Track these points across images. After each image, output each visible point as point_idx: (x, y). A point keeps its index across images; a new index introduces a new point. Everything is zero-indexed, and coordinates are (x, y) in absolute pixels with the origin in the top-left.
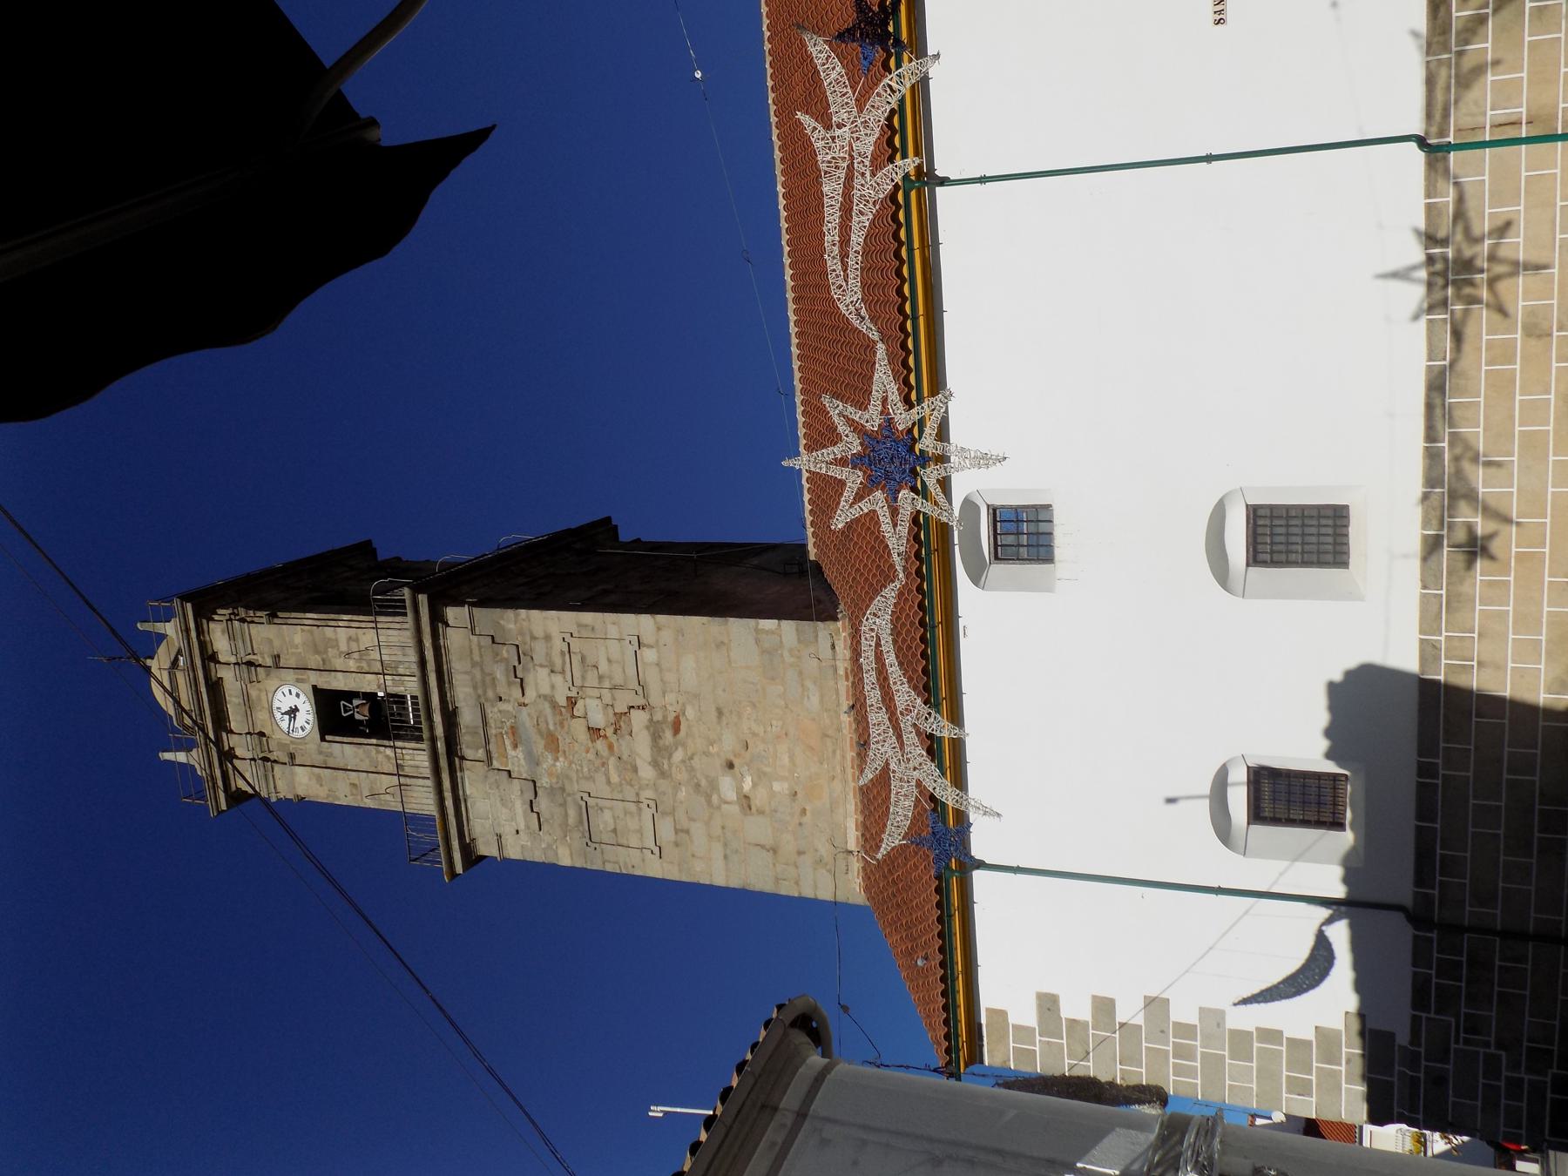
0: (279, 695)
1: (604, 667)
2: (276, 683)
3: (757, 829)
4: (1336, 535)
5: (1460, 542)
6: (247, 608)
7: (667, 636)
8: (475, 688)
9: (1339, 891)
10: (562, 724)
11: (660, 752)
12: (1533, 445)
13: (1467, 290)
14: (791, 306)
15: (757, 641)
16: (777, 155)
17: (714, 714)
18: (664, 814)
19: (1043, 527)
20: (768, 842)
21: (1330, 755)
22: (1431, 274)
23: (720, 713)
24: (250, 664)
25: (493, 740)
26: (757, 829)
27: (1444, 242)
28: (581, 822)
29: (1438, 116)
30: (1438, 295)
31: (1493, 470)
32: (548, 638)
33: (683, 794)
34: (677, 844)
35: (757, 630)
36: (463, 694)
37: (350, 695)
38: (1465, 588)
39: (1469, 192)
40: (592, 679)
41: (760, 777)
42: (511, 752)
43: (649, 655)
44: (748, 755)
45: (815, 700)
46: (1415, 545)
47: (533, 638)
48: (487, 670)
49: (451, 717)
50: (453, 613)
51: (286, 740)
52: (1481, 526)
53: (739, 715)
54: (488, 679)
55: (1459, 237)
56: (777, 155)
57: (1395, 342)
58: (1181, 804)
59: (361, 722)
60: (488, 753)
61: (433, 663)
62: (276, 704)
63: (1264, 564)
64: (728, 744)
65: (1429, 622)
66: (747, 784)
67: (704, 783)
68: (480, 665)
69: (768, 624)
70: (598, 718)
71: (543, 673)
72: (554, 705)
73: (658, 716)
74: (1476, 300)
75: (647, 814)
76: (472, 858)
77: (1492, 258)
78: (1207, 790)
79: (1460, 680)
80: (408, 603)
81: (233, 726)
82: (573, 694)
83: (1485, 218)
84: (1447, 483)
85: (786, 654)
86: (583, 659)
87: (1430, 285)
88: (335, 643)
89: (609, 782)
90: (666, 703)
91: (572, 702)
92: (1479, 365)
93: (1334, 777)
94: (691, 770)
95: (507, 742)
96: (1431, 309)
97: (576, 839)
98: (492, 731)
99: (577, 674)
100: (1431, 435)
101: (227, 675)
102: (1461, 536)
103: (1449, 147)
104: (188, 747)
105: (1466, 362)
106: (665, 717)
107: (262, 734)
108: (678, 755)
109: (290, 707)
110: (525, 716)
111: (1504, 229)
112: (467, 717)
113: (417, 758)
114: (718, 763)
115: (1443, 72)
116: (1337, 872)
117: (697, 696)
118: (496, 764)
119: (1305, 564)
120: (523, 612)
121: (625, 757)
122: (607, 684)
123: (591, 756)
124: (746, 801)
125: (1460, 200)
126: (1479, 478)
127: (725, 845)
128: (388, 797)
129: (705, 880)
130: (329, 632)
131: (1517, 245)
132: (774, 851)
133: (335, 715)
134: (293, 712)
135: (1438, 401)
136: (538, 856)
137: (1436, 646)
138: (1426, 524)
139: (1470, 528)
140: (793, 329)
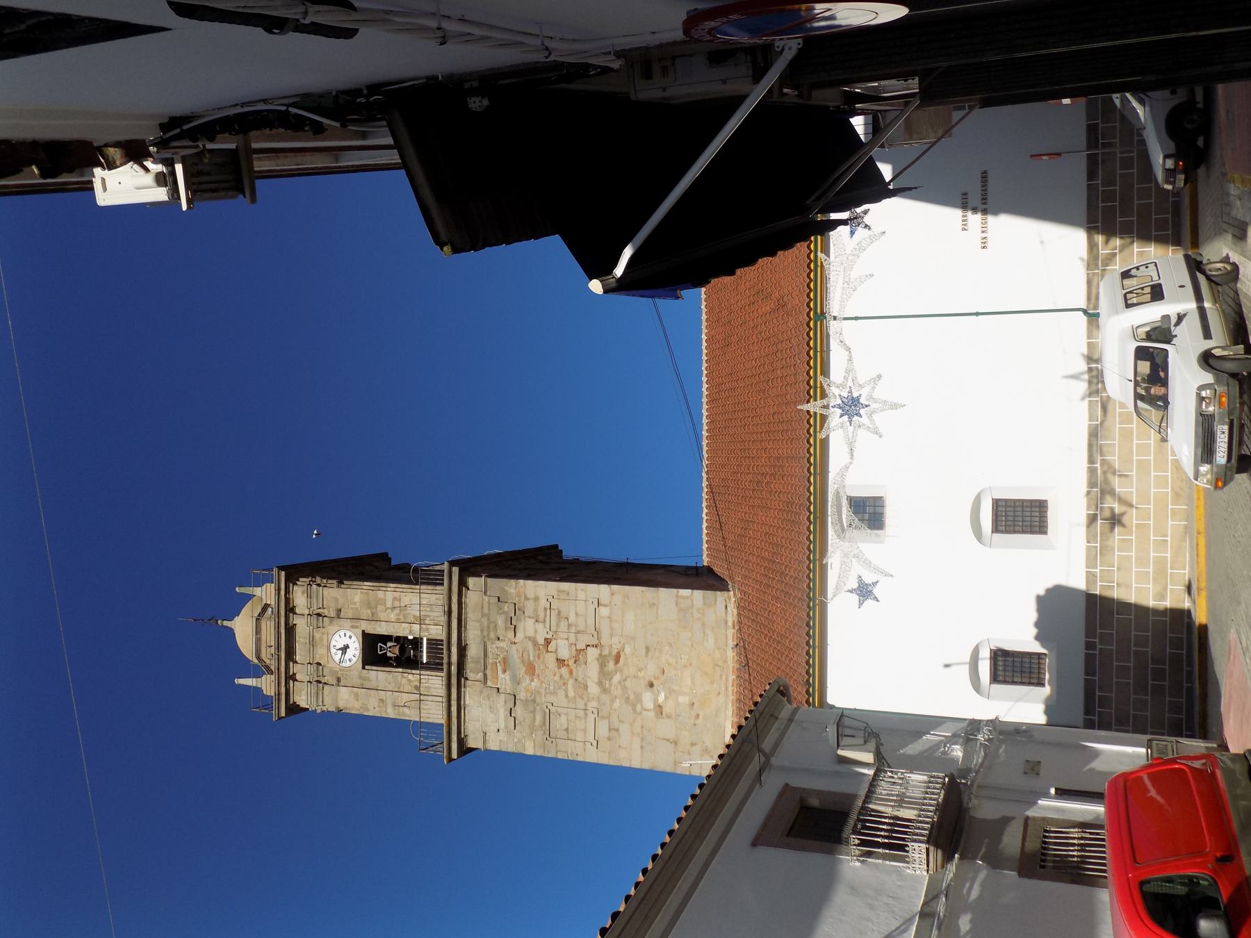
0: (336, 636)
1: (572, 619)
2: (336, 628)
3: (666, 728)
5: (1107, 518)
7: (618, 599)
8: (482, 631)
11: (604, 675)
12: (1143, 467)
14: (705, 406)
16: (704, 317)
17: (644, 651)
18: (603, 718)
20: (671, 736)
21: (1037, 638)
23: (648, 649)
24: (319, 615)
26: (666, 728)
28: (544, 724)
30: (1094, 387)
31: (1123, 479)
32: (536, 599)
33: (617, 704)
34: (609, 739)
35: (677, 596)
37: (385, 639)
38: (1109, 543)
41: (671, 693)
42: (501, 675)
43: (604, 611)
44: (663, 678)
45: (711, 641)
46: (1083, 519)
47: (526, 599)
49: (462, 650)
50: (472, 581)
52: (1118, 509)
53: (661, 652)
54: (492, 626)
56: (704, 317)
59: (391, 658)
61: (456, 615)
62: (333, 643)
63: (1001, 532)
64: (651, 671)
65: (1091, 561)
66: (661, 698)
67: (632, 697)
68: (488, 616)
69: (685, 592)
70: (564, 653)
71: (530, 623)
72: (535, 644)
73: (606, 652)
75: (591, 717)
76: (464, 750)
78: (968, 660)
79: (1108, 594)
80: (446, 573)
81: (298, 658)
82: (549, 636)
84: (1100, 486)
86: (559, 613)
87: (1090, 382)
88: (383, 602)
89: (567, 696)
90: (612, 642)
93: (1039, 655)
94: (625, 688)
95: (499, 668)
96: (1090, 395)
97: (539, 736)
98: (490, 661)
99: (554, 623)
100: (1091, 460)
101: (301, 624)
102: (1107, 514)
104: (257, 674)
105: (1106, 424)
106: (610, 653)
107: (319, 664)
108: (617, 678)
109: (344, 645)
110: (514, 652)
112: (473, 651)
113: (434, 682)
114: (643, 683)
116: (1042, 707)
117: (633, 638)
118: (489, 683)
119: (1023, 532)
120: (522, 581)
121: (580, 679)
122: (573, 630)
123: (557, 678)
124: (659, 709)
126: (1116, 483)
127: (642, 739)
128: (406, 710)
129: (626, 764)
130: (380, 594)
132: (676, 743)
133: (375, 651)
134: (345, 649)
136: (511, 748)
137: (1094, 575)
138: (1089, 508)
139: (1112, 509)
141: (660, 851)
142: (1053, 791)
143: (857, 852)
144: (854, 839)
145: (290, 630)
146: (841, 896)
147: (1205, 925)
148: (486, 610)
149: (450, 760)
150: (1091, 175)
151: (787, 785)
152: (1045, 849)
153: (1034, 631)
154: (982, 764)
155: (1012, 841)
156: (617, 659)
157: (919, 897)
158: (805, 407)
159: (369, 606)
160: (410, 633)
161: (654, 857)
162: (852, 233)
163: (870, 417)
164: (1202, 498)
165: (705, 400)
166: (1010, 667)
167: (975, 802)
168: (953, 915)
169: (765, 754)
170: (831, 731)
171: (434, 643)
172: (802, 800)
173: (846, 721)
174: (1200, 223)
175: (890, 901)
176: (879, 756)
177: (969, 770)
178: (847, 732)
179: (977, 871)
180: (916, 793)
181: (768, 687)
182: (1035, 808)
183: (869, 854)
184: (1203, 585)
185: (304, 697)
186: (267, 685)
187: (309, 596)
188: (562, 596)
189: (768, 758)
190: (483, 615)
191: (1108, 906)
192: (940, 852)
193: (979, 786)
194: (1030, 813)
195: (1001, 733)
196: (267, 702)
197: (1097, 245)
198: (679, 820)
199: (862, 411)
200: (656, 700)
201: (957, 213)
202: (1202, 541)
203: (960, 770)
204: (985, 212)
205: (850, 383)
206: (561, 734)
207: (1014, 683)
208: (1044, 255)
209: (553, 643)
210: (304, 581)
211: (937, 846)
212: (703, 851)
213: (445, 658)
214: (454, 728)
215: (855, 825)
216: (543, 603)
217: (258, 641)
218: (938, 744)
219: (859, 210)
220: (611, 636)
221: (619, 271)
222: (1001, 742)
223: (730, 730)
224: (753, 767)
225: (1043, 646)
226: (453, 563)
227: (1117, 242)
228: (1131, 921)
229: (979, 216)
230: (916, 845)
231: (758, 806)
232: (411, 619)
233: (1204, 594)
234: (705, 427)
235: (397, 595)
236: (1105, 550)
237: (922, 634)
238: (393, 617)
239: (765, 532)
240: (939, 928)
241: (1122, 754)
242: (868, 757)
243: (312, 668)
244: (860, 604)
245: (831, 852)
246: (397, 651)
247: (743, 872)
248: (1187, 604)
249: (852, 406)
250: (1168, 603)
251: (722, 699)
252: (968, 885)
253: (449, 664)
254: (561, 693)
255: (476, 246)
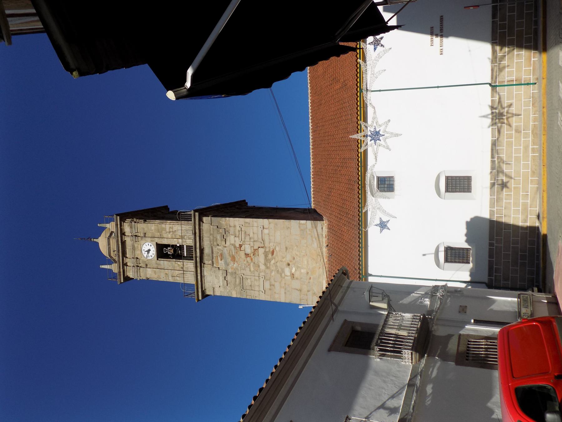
0: (144, 245)
1: (251, 235)
2: (144, 242)
3: (296, 284)
4: (468, 184)
5: (500, 184)
6: (137, 219)
7: (272, 226)
8: (210, 242)
9: (468, 279)
10: (237, 253)
11: (267, 260)
12: (517, 159)
13: (501, 120)
14: (311, 134)
15: (299, 227)
16: (309, 91)
18: (267, 280)
19: (391, 183)
20: (298, 288)
21: (466, 241)
22: (493, 116)
23: (286, 248)
24: (136, 236)
25: (214, 258)
26: (296, 284)
27: (496, 109)
28: (240, 283)
29: (494, 79)
30: (494, 121)
31: (508, 165)
32: (235, 226)
33: (273, 274)
34: (270, 289)
35: (299, 224)
36: (206, 244)
37: (167, 246)
38: (501, 196)
39: (502, 97)
40: (248, 238)
41: (298, 268)
42: (220, 262)
43: (266, 231)
44: (294, 262)
46: (488, 185)
47: (230, 226)
48: (215, 236)
49: (202, 251)
50: (205, 219)
51: (145, 260)
52: (505, 179)
54: (215, 239)
55: (499, 107)
56: (309, 91)
57: (484, 133)
58: (427, 256)
60: (213, 262)
61: (198, 235)
62: (143, 248)
64: (288, 258)
65: (492, 205)
66: (293, 271)
67: (280, 270)
69: (303, 222)
70: (248, 251)
71: (232, 237)
72: (235, 247)
73: (267, 250)
74: (503, 123)
75: (262, 280)
76: (205, 296)
77: (507, 112)
78: (434, 252)
79: (500, 220)
82: (241, 243)
83: (505, 103)
84: (496, 169)
85: (308, 231)
86: (245, 233)
87: (492, 119)
89: (250, 270)
90: (270, 245)
91: (241, 246)
92: (504, 140)
94: (276, 266)
95: (219, 259)
96: (492, 125)
97: (238, 289)
98: (215, 255)
99: (243, 237)
100: (493, 157)
101: (128, 240)
102: (500, 182)
103: (496, 86)
104: (110, 263)
105: (500, 139)
106: (269, 250)
107: (137, 258)
108: (273, 262)
109: (148, 249)
110: (226, 251)
111: (510, 106)
112: (207, 251)
113: (190, 265)
114: (285, 264)
115: (496, 68)
116: (468, 273)
117: (280, 244)
118: (215, 265)
120: (228, 219)
122: (252, 240)
123: (245, 262)
124: (293, 275)
125: (500, 98)
126: (504, 167)
127: (285, 289)
128: (178, 278)
130: (163, 226)
131: (513, 110)
132: (300, 290)
133: (163, 252)
134: (149, 251)
135: (494, 148)
136: (226, 294)
137: (493, 211)
138: (491, 179)
139: (502, 180)
140: (311, 141)
141: (283, 356)
142: (472, 321)
143: (378, 354)
144: (377, 348)
145: (123, 243)
146: (370, 376)
147: (549, 416)
148: (212, 232)
149: (198, 300)
150: (494, 16)
151: (346, 320)
152: (468, 350)
153: (465, 238)
154: (439, 308)
155: (452, 347)
156: (273, 253)
157: (407, 376)
158: (355, 136)
159: (158, 231)
160: (178, 243)
161: (281, 359)
162: (375, 49)
163: (385, 141)
164: (546, 174)
165: (311, 131)
166: (454, 255)
167: (435, 327)
168: (424, 384)
169: (335, 304)
170: (366, 294)
171: (189, 247)
172: (352, 327)
173: (374, 290)
174: (547, 39)
175: (394, 378)
176: (389, 305)
177: (433, 311)
178: (374, 294)
179: (436, 362)
180: (407, 323)
181: (337, 272)
182: (464, 330)
183: (383, 355)
184: (545, 216)
185: (131, 273)
186: (114, 268)
187: (131, 227)
188: (247, 225)
189: (337, 307)
190: (211, 234)
191: (498, 379)
192: (418, 354)
193: (437, 319)
194: (462, 332)
195: (448, 292)
196: (114, 276)
197: (496, 51)
198: (293, 340)
199: (381, 138)
200: (291, 271)
201: (428, 37)
202: (545, 195)
203: (428, 311)
204: (442, 36)
205: (375, 124)
206: (248, 288)
207: (455, 262)
208: (471, 56)
209: (243, 246)
210: (128, 220)
211: (416, 351)
212: (305, 353)
213: (193, 254)
214: (200, 286)
215: (377, 342)
216: (238, 228)
217: (109, 248)
218: (418, 298)
219: (378, 37)
220: (270, 242)
221: (188, 84)
222: (449, 296)
223: (325, 285)
224: (330, 312)
225: (469, 245)
226: (195, 211)
227: (506, 49)
228: (511, 413)
229: (438, 39)
230: (406, 351)
231: (332, 330)
232: (178, 237)
233: (545, 220)
234: (311, 144)
235: (171, 226)
236: (499, 200)
237: (412, 245)
238: (170, 236)
239: (340, 195)
240: (417, 392)
241: (505, 301)
242: (385, 306)
243: (134, 260)
244: (381, 231)
245: (367, 354)
246: (172, 251)
247: (323, 364)
248: (537, 224)
249: (376, 136)
250: (528, 224)
251: (321, 270)
252: (431, 369)
253: (196, 257)
254: (248, 269)
255: (100, 70)
